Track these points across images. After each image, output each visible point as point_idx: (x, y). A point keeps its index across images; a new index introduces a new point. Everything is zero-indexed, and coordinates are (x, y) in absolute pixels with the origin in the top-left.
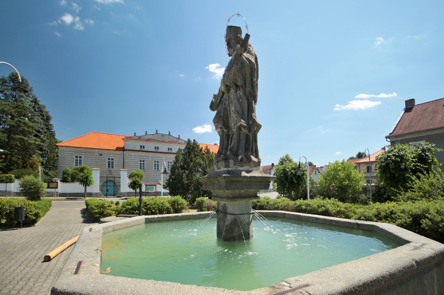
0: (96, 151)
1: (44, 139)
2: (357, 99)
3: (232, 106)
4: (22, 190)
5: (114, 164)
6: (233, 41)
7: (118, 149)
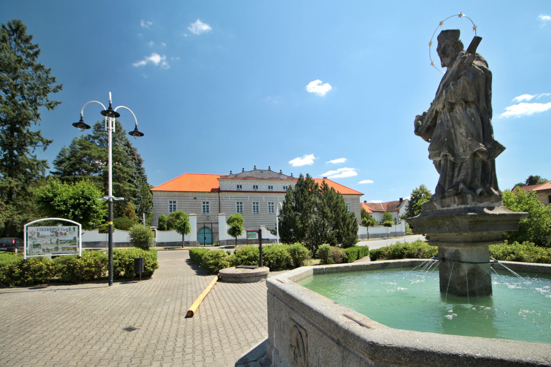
0: (190, 194)
1: (137, 184)
2: (517, 103)
3: (460, 127)
4: (131, 240)
5: (210, 208)
6: (451, 48)
7: (213, 191)
